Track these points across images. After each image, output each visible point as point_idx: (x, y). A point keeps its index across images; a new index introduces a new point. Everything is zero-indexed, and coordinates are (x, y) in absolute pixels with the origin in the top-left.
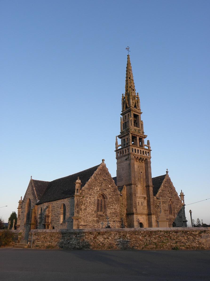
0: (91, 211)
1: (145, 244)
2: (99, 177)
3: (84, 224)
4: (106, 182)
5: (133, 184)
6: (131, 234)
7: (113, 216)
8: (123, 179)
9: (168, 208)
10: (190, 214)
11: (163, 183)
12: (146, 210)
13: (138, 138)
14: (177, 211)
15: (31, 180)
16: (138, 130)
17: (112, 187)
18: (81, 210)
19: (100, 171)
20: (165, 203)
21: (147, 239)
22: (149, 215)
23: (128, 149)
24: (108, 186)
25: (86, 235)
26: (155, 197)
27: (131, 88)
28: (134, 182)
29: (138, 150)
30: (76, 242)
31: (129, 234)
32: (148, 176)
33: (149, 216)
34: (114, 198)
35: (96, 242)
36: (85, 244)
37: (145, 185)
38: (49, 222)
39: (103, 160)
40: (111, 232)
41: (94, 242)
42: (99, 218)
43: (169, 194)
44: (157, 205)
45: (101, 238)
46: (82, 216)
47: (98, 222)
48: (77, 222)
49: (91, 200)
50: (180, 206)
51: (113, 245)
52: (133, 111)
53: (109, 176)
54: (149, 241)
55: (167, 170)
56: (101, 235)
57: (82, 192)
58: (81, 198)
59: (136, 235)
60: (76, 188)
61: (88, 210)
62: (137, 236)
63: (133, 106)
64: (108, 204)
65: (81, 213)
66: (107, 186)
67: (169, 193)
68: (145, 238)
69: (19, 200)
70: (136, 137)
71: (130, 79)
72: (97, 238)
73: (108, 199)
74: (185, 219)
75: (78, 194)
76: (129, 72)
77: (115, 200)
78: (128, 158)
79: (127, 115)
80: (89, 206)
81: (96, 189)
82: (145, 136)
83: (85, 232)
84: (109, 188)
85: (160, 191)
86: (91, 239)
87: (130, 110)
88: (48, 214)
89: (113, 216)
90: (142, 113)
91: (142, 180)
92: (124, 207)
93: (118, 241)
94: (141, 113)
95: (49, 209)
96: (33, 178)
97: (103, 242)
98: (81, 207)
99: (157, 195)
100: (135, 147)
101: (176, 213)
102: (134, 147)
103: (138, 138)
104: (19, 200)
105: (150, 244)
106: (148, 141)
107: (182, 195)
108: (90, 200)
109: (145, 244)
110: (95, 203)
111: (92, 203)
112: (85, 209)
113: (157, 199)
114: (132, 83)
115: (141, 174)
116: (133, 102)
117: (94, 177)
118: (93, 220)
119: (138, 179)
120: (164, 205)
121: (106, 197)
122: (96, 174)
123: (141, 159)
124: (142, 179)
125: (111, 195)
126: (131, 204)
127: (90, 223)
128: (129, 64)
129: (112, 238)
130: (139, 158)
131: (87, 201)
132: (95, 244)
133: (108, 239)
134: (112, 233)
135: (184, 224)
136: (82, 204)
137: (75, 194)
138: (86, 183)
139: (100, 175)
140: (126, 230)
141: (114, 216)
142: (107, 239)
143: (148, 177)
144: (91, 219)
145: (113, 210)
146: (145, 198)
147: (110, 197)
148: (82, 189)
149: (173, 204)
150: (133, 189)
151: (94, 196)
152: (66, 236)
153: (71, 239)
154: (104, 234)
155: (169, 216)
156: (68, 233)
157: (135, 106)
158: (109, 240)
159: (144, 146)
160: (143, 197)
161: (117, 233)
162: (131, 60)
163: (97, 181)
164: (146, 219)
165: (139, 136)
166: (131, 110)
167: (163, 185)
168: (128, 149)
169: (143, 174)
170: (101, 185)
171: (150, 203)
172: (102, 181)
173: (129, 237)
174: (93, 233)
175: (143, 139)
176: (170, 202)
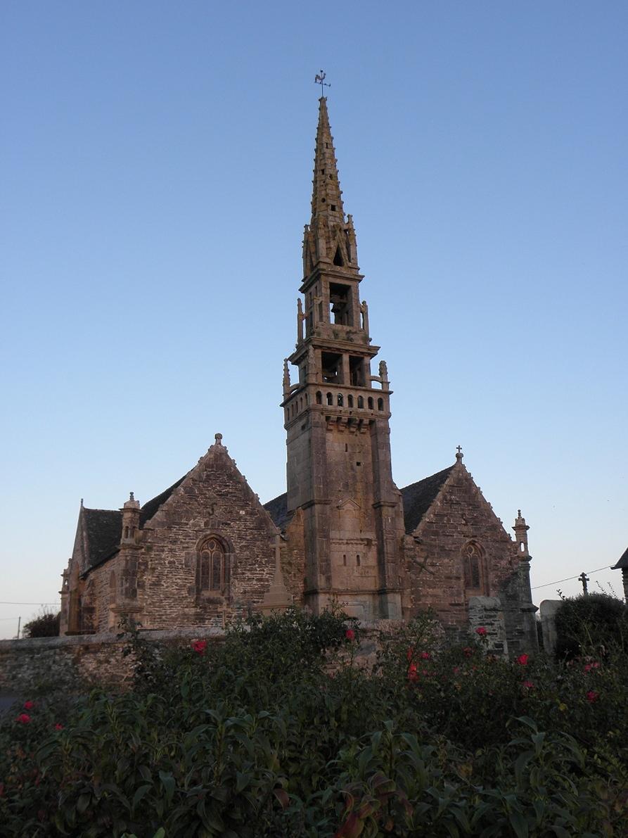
0: (176, 589)
2: (204, 487)
3: (152, 626)
7: (254, 602)
8: (298, 487)
10: (583, 587)
13: (346, 358)
15: (81, 512)
16: (348, 333)
18: (141, 586)
19: (206, 470)
20: (448, 555)
22: (381, 593)
24: (234, 512)
25: (55, 653)
26: (409, 539)
27: (325, 203)
28: (322, 494)
29: (350, 398)
30: (31, 674)
35: (78, 673)
38: (93, 625)
39: (218, 437)
42: (204, 608)
45: (91, 662)
46: (145, 604)
49: (174, 556)
50: (510, 563)
51: (118, 681)
53: (239, 482)
55: (459, 448)
56: (92, 653)
57: (145, 535)
58: (142, 554)
60: (124, 524)
61: (167, 587)
63: (328, 260)
64: (236, 567)
65: (142, 595)
67: (463, 522)
69: (65, 570)
71: (324, 176)
72: (82, 660)
73: (237, 552)
74: (528, 602)
75: (129, 541)
76: (322, 152)
77: (263, 552)
79: (312, 289)
81: (194, 525)
82: (370, 348)
84: (239, 520)
85: (428, 517)
86: (66, 664)
87: (316, 275)
89: (254, 602)
90: (363, 277)
91: (359, 486)
92: (295, 574)
94: (359, 279)
95: (92, 590)
96: (87, 506)
97: (95, 672)
98: (141, 580)
101: (494, 586)
103: (346, 358)
104: (65, 570)
106: (383, 365)
108: (171, 557)
110: (189, 566)
111: (180, 566)
112: (156, 584)
113: (418, 543)
114: (329, 187)
115: (357, 471)
116: (329, 249)
117: (185, 488)
118: (185, 614)
119: (346, 485)
120: (446, 560)
123: (352, 424)
124: (359, 484)
127: (172, 623)
128: (323, 127)
131: (161, 559)
133: (108, 662)
134: (119, 645)
135: (525, 619)
136: (144, 570)
138: (159, 509)
139: (206, 481)
140: (154, 637)
141: (258, 602)
142: (106, 665)
143: (379, 478)
144: (176, 611)
145: (255, 582)
148: (146, 526)
149: (483, 558)
151: (186, 545)
152: (9, 658)
153: (21, 666)
155: (462, 596)
157: (338, 261)
158: (109, 666)
160: (362, 540)
164: (374, 607)
165: (347, 351)
166: (320, 274)
169: (365, 467)
170: (211, 512)
172: (215, 498)
174: (71, 648)
175: (366, 359)
176: (473, 552)
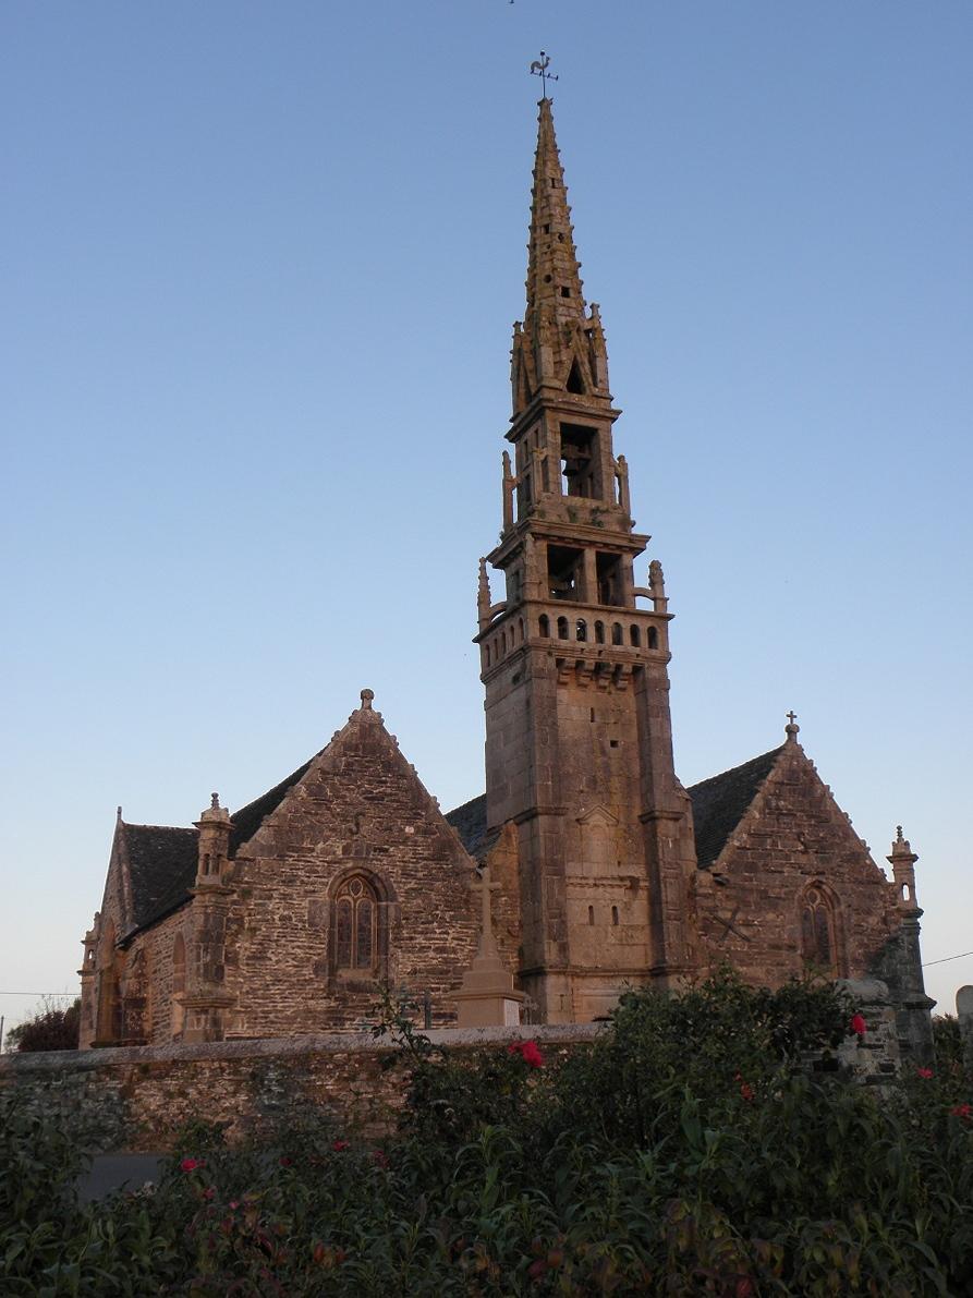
0: (295, 966)
1: (351, 1117)
3: (250, 1031)
4: (387, 807)
5: (540, 810)
6: (285, 1067)
7: (432, 989)
9: (798, 935)
11: (757, 796)
12: (640, 950)
13: (590, 556)
14: (867, 946)
16: (594, 511)
17: (426, 832)
18: (233, 959)
19: (345, 755)
21: (362, 1090)
23: (521, 620)
24: (395, 829)
26: (705, 878)
31: (281, 1066)
32: (650, 762)
33: (660, 978)
34: (438, 892)
35: (129, 1115)
36: (81, 1127)
37: (637, 812)
38: (142, 1030)
40: (198, 1064)
41: (124, 1115)
42: (343, 1000)
43: (804, 852)
44: (715, 918)
46: (238, 993)
47: (335, 1019)
48: (203, 1022)
49: (290, 907)
50: (884, 921)
52: (555, 409)
53: (403, 776)
54: (371, 1101)
55: (792, 716)
57: (238, 870)
58: (234, 902)
59: (311, 1072)
61: (277, 962)
62: (313, 1077)
63: (556, 384)
66: (390, 829)
67: (801, 848)
68: (352, 1085)
69: (88, 933)
70: (578, 554)
72: (137, 1091)
73: (401, 899)
76: (545, 194)
78: (524, 668)
79: (530, 434)
80: (283, 941)
81: (325, 852)
83: (84, 1064)
84: (404, 843)
85: (738, 838)
86: (109, 1098)
88: (139, 991)
90: (619, 412)
91: (616, 783)
93: (227, 1104)
94: (613, 416)
97: (160, 1112)
98: (231, 949)
99: (714, 862)
100: (562, 606)
102: (554, 610)
103: (590, 556)
104: (88, 933)
105: (373, 1119)
106: (655, 568)
107: (903, 858)
109: (351, 1117)
111: (300, 925)
112: (259, 957)
114: (558, 255)
116: (559, 363)
117: (308, 788)
119: (593, 782)
121: (384, 887)
122: (323, 772)
125: (420, 875)
126: (535, 922)
128: (546, 150)
129: (200, 1093)
130: (593, 668)
132: (125, 1123)
133: (183, 1094)
134: (204, 1065)
135: (912, 1021)
136: (237, 933)
137: (197, 883)
141: (438, 989)
142: (180, 1099)
143: (651, 768)
144: (293, 1005)
145: (431, 954)
146: (634, 885)
147: (409, 886)
148: (240, 853)
150: (542, 841)
154: (167, 1075)
156: (14, 1074)
157: (575, 384)
159: (629, 598)
160: (622, 879)
161: (224, 1064)
162: (558, 126)
163: (329, 809)
167: (761, 803)
168: (521, 620)
169: (626, 750)
170: (354, 829)
171: (661, 911)
173: (280, 1083)
175: (626, 558)
